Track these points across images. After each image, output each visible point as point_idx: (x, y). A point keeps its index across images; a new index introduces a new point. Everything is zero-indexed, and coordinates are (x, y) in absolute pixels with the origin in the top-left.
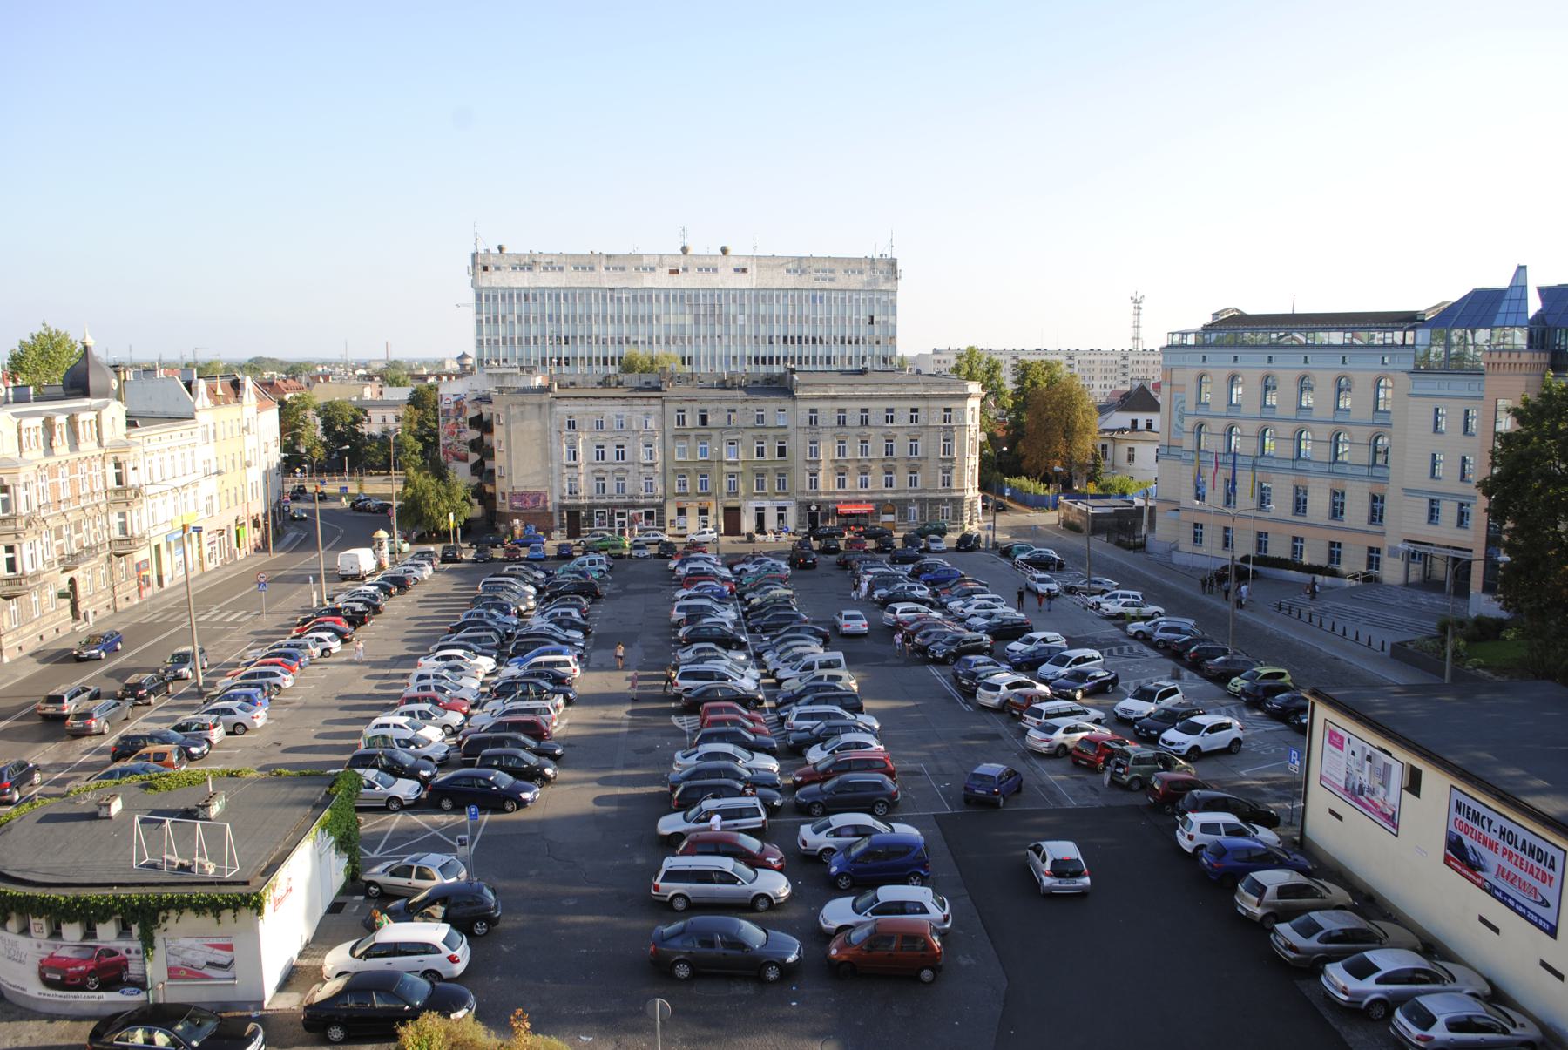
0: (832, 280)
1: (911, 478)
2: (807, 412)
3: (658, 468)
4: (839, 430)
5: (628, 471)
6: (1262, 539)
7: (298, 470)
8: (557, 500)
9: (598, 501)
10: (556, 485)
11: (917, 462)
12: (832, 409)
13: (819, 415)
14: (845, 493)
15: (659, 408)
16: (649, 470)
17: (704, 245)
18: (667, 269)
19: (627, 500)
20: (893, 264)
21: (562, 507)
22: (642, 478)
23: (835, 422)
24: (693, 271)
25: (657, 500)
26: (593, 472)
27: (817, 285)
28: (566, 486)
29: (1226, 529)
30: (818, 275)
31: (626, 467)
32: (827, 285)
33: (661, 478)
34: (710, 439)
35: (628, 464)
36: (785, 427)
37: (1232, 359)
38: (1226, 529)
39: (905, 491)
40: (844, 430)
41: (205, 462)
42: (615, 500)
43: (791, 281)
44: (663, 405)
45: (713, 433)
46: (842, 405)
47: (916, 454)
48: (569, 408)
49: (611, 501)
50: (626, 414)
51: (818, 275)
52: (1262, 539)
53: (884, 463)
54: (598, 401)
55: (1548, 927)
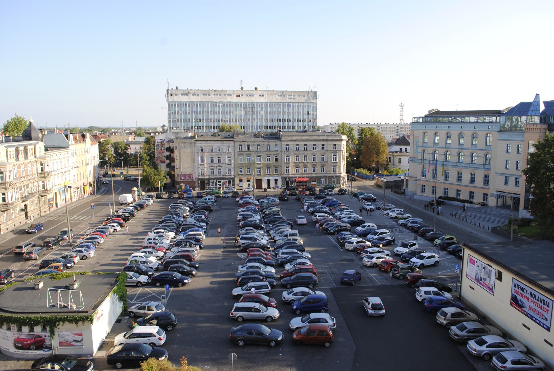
0: (294, 99)
1: (322, 169)
2: (285, 146)
3: (233, 165)
4: (296, 152)
5: (222, 166)
6: (446, 190)
7: (105, 166)
8: (197, 177)
9: (211, 177)
10: (196, 171)
11: (324, 163)
12: (294, 144)
13: (290, 146)
14: (299, 174)
15: (233, 144)
16: (229, 166)
17: (249, 87)
18: (236, 95)
19: (221, 177)
20: (315, 93)
21: (199, 179)
22: (227, 169)
23: (295, 149)
24: (245, 96)
25: (232, 177)
26: (210, 167)
27: (289, 101)
28: (200, 172)
29: (433, 187)
30: (289, 97)
31: (221, 165)
32: (292, 101)
33: (234, 169)
34: (251, 155)
35: (222, 164)
36: (277, 151)
37: (435, 127)
38: (433, 187)
39: (320, 173)
40: (298, 152)
41: (72, 163)
42: (217, 177)
43: (279, 99)
44: (234, 143)
45: (252, 153)
46: (297, 143)
47: (324, 160)
48: (201, 144)
49: (216, 177)
50: (221, 146)
51: (289, 97)
52: (446, 190)
53: (312, 164)
54: (211, 142)
55: (547, 328)
